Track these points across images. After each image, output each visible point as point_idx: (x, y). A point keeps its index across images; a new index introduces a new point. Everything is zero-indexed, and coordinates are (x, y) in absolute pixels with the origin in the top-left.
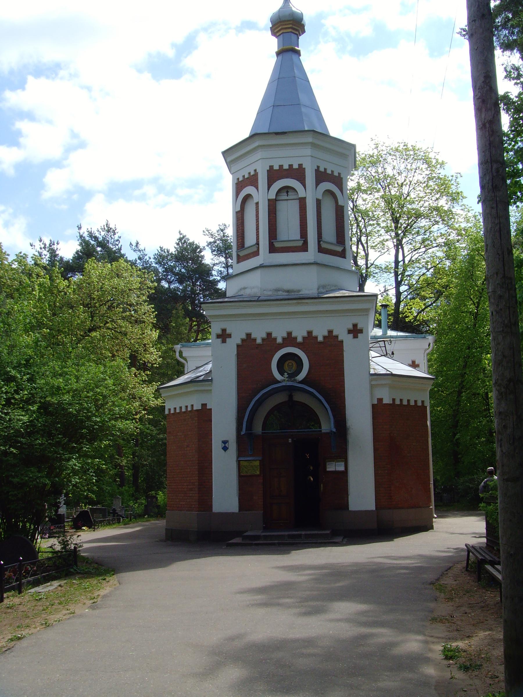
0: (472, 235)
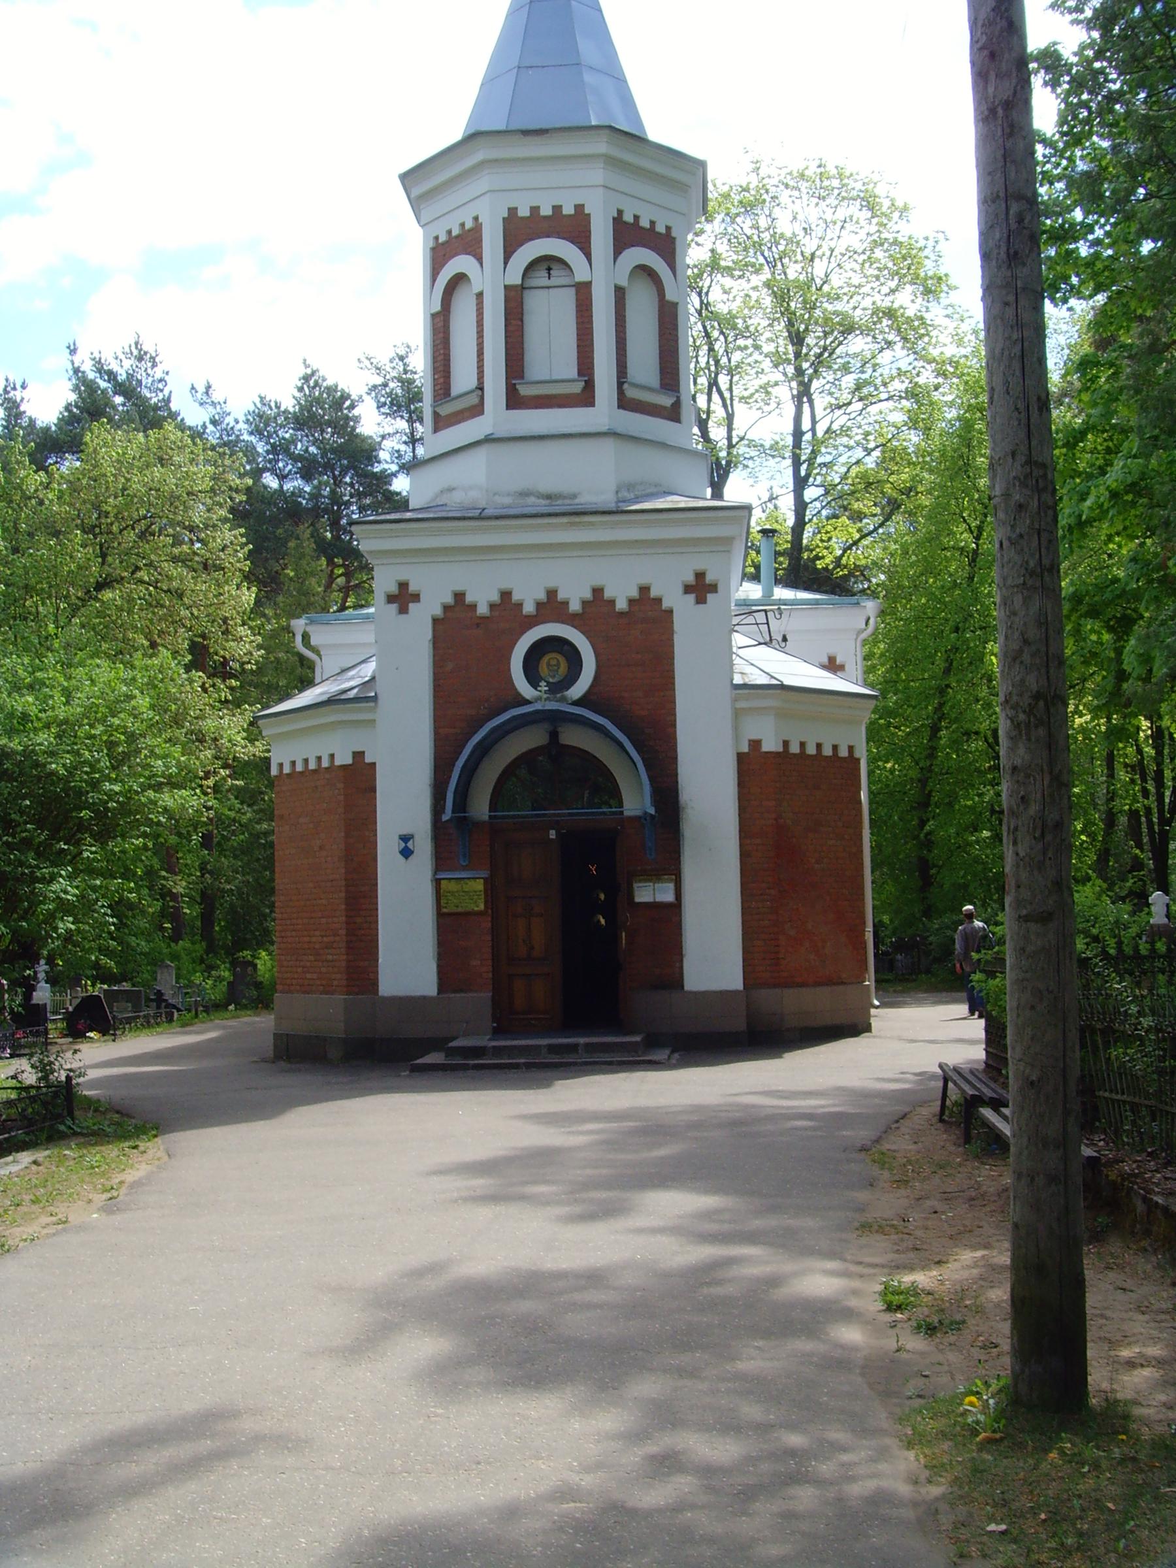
0: (969, 374)
